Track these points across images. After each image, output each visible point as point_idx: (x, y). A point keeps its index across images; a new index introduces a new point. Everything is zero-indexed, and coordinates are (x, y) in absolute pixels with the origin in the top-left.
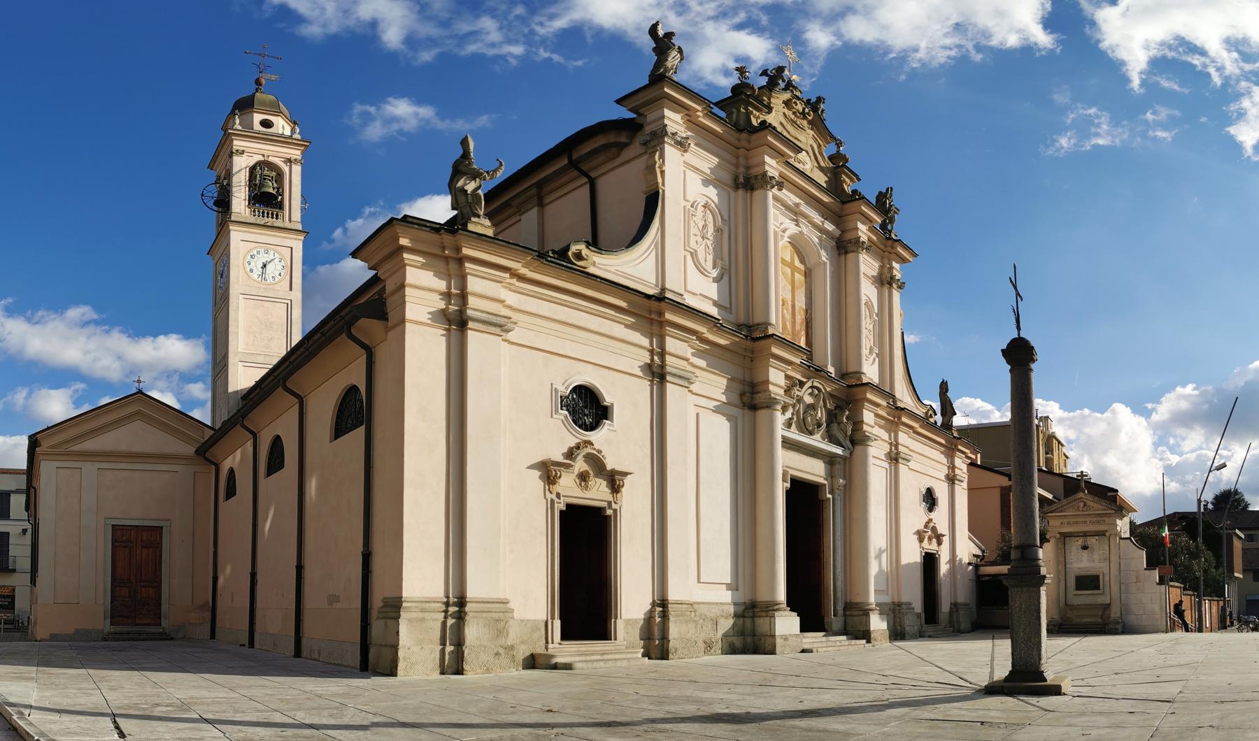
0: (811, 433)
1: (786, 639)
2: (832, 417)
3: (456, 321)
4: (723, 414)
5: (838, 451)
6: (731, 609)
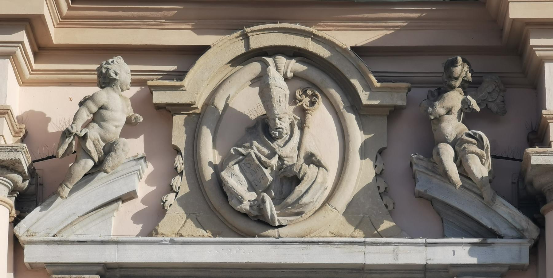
3: (520, 244)
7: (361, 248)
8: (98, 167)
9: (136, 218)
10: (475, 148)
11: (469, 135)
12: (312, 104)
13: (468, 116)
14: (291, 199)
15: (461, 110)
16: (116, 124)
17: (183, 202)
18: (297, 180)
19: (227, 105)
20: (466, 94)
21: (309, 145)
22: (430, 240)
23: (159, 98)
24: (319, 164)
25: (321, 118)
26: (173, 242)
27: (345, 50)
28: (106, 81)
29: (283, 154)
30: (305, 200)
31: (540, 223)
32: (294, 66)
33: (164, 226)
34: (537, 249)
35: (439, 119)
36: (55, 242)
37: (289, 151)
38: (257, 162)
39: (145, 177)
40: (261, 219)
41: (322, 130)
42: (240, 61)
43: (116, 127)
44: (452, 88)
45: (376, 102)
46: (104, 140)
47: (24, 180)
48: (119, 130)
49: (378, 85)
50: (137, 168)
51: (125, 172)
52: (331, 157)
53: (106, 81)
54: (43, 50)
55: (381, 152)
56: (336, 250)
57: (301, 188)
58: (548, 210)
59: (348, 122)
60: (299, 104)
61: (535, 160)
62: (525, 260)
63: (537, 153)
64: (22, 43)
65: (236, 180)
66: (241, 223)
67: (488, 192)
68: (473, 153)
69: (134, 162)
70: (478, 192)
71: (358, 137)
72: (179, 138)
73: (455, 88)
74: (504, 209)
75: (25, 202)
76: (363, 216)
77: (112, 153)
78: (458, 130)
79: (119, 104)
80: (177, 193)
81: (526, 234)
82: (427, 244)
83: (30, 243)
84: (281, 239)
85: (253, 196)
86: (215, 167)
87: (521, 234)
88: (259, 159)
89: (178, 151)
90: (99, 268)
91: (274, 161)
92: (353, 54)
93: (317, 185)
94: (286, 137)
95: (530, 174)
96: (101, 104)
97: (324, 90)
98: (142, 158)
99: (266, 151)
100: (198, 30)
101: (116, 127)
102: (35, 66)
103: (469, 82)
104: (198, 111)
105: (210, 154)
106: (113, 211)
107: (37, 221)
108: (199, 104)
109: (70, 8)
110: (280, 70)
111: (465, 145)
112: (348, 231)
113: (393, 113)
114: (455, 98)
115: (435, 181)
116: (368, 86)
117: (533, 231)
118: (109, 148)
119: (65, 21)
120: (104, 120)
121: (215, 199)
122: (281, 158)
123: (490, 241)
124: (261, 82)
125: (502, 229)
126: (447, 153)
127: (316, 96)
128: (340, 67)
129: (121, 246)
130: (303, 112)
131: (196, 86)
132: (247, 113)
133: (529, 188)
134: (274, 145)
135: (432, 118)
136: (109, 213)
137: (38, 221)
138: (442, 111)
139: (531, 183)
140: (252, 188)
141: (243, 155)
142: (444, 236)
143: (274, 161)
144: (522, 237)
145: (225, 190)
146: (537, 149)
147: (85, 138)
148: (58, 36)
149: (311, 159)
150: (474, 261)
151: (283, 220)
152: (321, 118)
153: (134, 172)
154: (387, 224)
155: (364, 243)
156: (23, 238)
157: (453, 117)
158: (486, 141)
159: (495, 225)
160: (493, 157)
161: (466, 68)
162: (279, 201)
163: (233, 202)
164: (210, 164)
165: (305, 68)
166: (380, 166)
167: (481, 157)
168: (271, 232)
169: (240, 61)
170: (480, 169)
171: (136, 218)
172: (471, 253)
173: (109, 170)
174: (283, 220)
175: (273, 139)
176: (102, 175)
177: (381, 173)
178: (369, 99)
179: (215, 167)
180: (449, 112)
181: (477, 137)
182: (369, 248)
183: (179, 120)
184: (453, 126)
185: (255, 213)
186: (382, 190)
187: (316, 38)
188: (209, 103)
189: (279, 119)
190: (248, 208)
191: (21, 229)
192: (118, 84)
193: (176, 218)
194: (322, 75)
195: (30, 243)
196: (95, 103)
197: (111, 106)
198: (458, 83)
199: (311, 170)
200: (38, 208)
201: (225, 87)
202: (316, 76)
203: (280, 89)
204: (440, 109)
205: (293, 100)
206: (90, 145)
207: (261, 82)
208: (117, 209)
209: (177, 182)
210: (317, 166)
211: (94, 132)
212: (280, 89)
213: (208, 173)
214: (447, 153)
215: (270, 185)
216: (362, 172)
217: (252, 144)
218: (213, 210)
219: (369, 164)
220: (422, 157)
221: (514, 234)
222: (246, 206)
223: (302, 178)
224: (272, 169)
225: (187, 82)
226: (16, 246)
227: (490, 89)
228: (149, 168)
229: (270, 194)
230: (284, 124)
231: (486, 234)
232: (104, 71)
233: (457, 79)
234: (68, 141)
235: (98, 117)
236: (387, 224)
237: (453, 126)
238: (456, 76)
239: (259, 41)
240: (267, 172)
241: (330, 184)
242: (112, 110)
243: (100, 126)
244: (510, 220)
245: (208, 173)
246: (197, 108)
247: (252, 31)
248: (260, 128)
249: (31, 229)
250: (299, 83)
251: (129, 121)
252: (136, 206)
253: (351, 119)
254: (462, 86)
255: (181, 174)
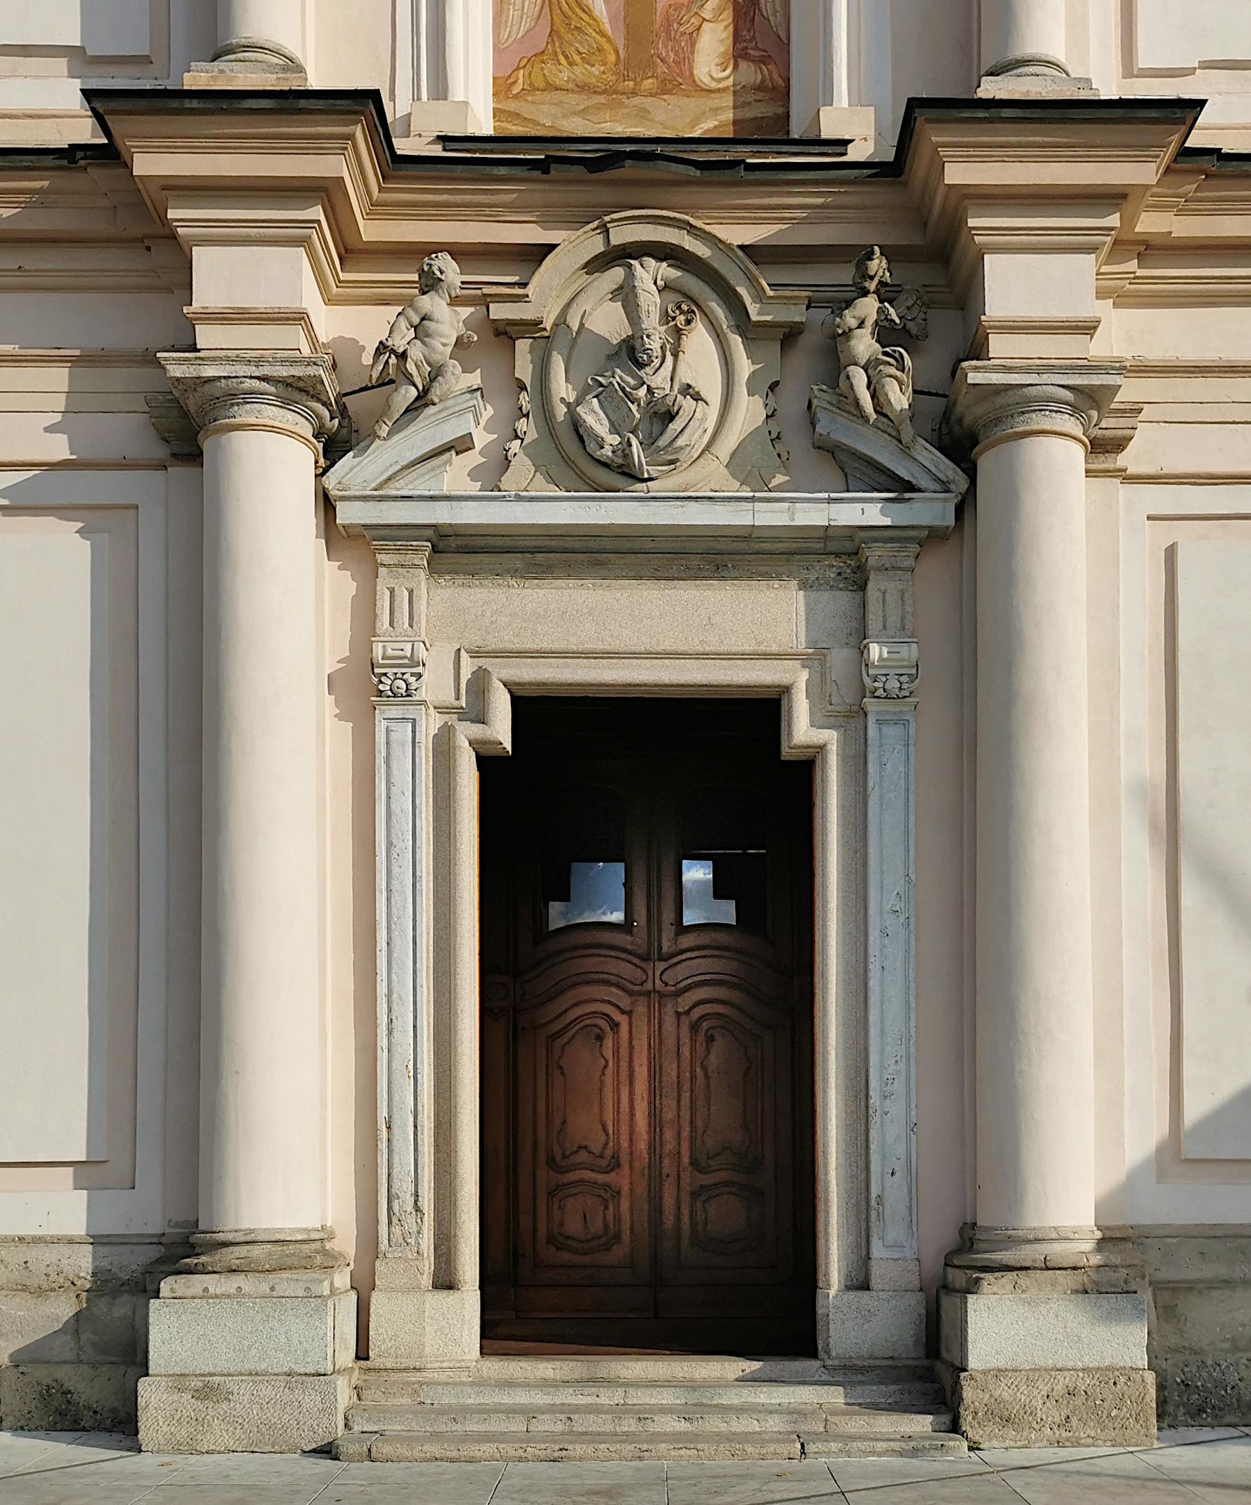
0: (628, 473)
1: (208, 1391)
2: (801, 352)
3: (945, 500)
4: (63, 511)
5: (866, 511)
6: (83, 1262)
7: (749, 506)
8: (422, 400)
9: (474, 474)
10: (893, 371)
11: (886, 354)
12: (688, 322)
13: (886, 334)
14: (662, 442)
15: (876, 323)
16: (444, 341)
17: (527, 450)
18: (670, 416)
19: (582, 325)
20: (881, 301)
21: (684, 376)
22: (833, 495)
23: (499, 312)
24: (697, 398)
25: (699, 340)
26: (519, 498)
27: (729, 246)
28: (430, 283)
29: (653, 385)
30: (680, 442)
31: (971, 472)
32: (666, 271)
33: (510, 482)
34: (965, 506)
35: (848, 334)
36: (372, 498)
37: (660, 380)
38: (620, 393)
39: (483, 422)
40: (626, 470)
41: (700, 360)
42: (597, 265)
43: (444, 345)
44: (865, 293)
45: (768, 318)
46: (429, 364)
47: (332, 418)
48: (449, 350)
49: (771, 293)
50: (471, 403)
51: (457, 409)
52: (712, 389)
53: (430, 283)
54: (351, 252)
55: (773, 387)
56: (719, 508)
57: (675, 426)
58: (982, 452)
59: (733, 346)
60: (672, 324)
61: (973, 378)
62: (951, 521)
63: (976, 368)
64: (318, 222)
65: (595, 419)
66: (602, 475)
67: (907, 432)
68: (891, 376)
69: (468, 396)
70: (894, 433)
71: (744, 367)
72: (524, 369)
73: (868, 292)
74: (925, 453)
75: (334, 447)
76: (750, 470)
77: (440, 378)
78: (871, 350)
79: (450, 322)
80: (523, 440)
81: (952, 487)
82: (830, 501)
83: (343, 498)
84: (650, 494)
85: (615, 440)
86: (568, 405)
87: (945, 487)
88: (623, 390)
89: (523, 388)
90: (430, 533)
91: (642, 392)
92: (740, 253)
93: (695, 426)
94: (657, 362)
95: (963, 400)
96: (424, 312)
97: (701, 303)
98: (477, 390)
99: (632, 382)
100: (543, 223)
101: (444, 345)
102: (343, 276)
103: (886, 284)
104: (545, 334)
105: (562, 389)
106: (446, 463)
107: (353, 471)
108: (548, 324)
109: (381, 190)
110: (648, 274)
111: (881, 367)
112: (733, 488)
113: (789, 335)
114: (869, 307)
115: (840, 419)
116: (759, 296)
117: (962, 483)
118: (436, 373)
119: (376, 209)
120: (428, 335)
121: (571, 446)
122: (649, 389)
123: (907, 495)
124: (626, 294)
125: (922, 481)
126: (859, 379)
127: (693, 312)
128: (723, 271)
129: (454, 503)
130: (678, 332)
131: (545, 294)
132: (607, 336)
133: (956, 429)
134: (642, 373)
135: (840, 331)
136: (439, 467)
137: (351, 470)
138: (853, 323)
139: (960, 421)
140: (614, 429)
141: (601, 385)
142: (848, 491)
143: (642, 392)
144: (947, 491)
145: (581, 431)
146: (974, 363)
147: (403, 356)
148: (371, 231)
149: (687, 390)
150: (887, 521)
151: (653, 471)
152: (699, 340)
153: (467, 410)
154: (780, 479)
155: (753, 499)
156: (333, 493)
157: (867, 331)
158: (908, 361)
159: (914, 477)
160: (915, 391)
161: (884, 264)
162: (649, 444)
163: (591, 447)
164: (562, 400)
165: (680, 274)
166: (772, 405)
167: (900, 383)
168: (639, 486)
169: (597, 265)
170: (899, 399)
171: (474, 474)
172: (883, 512)
173: (436, 400)
174: (653, 471)
175: (641, 366)
176: (431, 410)
177: (772, 415)
178: (759, 314)
179: (568, 405)
180: (861, 325)
181: (897, 355)
182: (759, 506)
183: (523, 345)
184: (864, 345)
185: (620, 461)
186: (774, 435)
187: (691, 229)
188: (561, 322)
189: (648, 336)
190: (610, 454)
191: (330, 481)
192: (444, 285)
193: (522, 470)
194: (703, 282)
195: (343, 498)
196: (416, 310)
197: (436, 316)
198: (872, 286)
199: (688, 404)
200: (351, 454)
201: (578, 300)
202: (694, 285)
203: (650, 301)
204: (850, 319)
205: (666, 318)
206: (411, 367)
207: (626, 294)
208: (449, 462)
209: (522, 425)
210: (696, 400)
211: (416, 352)
212: (650, 301)
213: (561, 411)
214: (859, 379)
215: (638, 424)
216: (749, 412)
217: (614, 372)
218: (569, 463)
219: (758, 401)
220: (824, 387)
221: (938, 487)
222: (608, 451)
223: (677, 413)
224: (639, 405)
225: (529, 291)
226: (326, 504)
227: (910, 302)
228: (488, 412)
229: (637, 437)
230: (655, 345)
231: (903, 488)
232: (426, 268)
233: (872, 278)
234: (383, 358)
235: (421, 330)
236: (780, 479)
237: (864, 345)
238: (872, 273)
239: (623, 235)
240: (634, 408)
241: (711, 425)
242: (438, 322)
243: (423, 343)
244: (933, 469)
245: (561, 411)
246: (545, 329)
247: (613, 221)
248: (624, 354)
249: (344, 481)
250: (674, 297)
251: (459, 342)
252: (473, 459)
253: (736, 341)
254: (876, 292)
255: (527, 415)
